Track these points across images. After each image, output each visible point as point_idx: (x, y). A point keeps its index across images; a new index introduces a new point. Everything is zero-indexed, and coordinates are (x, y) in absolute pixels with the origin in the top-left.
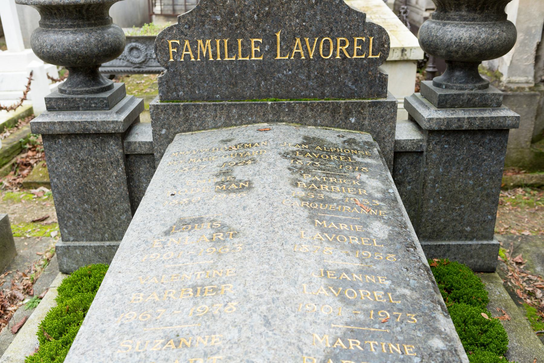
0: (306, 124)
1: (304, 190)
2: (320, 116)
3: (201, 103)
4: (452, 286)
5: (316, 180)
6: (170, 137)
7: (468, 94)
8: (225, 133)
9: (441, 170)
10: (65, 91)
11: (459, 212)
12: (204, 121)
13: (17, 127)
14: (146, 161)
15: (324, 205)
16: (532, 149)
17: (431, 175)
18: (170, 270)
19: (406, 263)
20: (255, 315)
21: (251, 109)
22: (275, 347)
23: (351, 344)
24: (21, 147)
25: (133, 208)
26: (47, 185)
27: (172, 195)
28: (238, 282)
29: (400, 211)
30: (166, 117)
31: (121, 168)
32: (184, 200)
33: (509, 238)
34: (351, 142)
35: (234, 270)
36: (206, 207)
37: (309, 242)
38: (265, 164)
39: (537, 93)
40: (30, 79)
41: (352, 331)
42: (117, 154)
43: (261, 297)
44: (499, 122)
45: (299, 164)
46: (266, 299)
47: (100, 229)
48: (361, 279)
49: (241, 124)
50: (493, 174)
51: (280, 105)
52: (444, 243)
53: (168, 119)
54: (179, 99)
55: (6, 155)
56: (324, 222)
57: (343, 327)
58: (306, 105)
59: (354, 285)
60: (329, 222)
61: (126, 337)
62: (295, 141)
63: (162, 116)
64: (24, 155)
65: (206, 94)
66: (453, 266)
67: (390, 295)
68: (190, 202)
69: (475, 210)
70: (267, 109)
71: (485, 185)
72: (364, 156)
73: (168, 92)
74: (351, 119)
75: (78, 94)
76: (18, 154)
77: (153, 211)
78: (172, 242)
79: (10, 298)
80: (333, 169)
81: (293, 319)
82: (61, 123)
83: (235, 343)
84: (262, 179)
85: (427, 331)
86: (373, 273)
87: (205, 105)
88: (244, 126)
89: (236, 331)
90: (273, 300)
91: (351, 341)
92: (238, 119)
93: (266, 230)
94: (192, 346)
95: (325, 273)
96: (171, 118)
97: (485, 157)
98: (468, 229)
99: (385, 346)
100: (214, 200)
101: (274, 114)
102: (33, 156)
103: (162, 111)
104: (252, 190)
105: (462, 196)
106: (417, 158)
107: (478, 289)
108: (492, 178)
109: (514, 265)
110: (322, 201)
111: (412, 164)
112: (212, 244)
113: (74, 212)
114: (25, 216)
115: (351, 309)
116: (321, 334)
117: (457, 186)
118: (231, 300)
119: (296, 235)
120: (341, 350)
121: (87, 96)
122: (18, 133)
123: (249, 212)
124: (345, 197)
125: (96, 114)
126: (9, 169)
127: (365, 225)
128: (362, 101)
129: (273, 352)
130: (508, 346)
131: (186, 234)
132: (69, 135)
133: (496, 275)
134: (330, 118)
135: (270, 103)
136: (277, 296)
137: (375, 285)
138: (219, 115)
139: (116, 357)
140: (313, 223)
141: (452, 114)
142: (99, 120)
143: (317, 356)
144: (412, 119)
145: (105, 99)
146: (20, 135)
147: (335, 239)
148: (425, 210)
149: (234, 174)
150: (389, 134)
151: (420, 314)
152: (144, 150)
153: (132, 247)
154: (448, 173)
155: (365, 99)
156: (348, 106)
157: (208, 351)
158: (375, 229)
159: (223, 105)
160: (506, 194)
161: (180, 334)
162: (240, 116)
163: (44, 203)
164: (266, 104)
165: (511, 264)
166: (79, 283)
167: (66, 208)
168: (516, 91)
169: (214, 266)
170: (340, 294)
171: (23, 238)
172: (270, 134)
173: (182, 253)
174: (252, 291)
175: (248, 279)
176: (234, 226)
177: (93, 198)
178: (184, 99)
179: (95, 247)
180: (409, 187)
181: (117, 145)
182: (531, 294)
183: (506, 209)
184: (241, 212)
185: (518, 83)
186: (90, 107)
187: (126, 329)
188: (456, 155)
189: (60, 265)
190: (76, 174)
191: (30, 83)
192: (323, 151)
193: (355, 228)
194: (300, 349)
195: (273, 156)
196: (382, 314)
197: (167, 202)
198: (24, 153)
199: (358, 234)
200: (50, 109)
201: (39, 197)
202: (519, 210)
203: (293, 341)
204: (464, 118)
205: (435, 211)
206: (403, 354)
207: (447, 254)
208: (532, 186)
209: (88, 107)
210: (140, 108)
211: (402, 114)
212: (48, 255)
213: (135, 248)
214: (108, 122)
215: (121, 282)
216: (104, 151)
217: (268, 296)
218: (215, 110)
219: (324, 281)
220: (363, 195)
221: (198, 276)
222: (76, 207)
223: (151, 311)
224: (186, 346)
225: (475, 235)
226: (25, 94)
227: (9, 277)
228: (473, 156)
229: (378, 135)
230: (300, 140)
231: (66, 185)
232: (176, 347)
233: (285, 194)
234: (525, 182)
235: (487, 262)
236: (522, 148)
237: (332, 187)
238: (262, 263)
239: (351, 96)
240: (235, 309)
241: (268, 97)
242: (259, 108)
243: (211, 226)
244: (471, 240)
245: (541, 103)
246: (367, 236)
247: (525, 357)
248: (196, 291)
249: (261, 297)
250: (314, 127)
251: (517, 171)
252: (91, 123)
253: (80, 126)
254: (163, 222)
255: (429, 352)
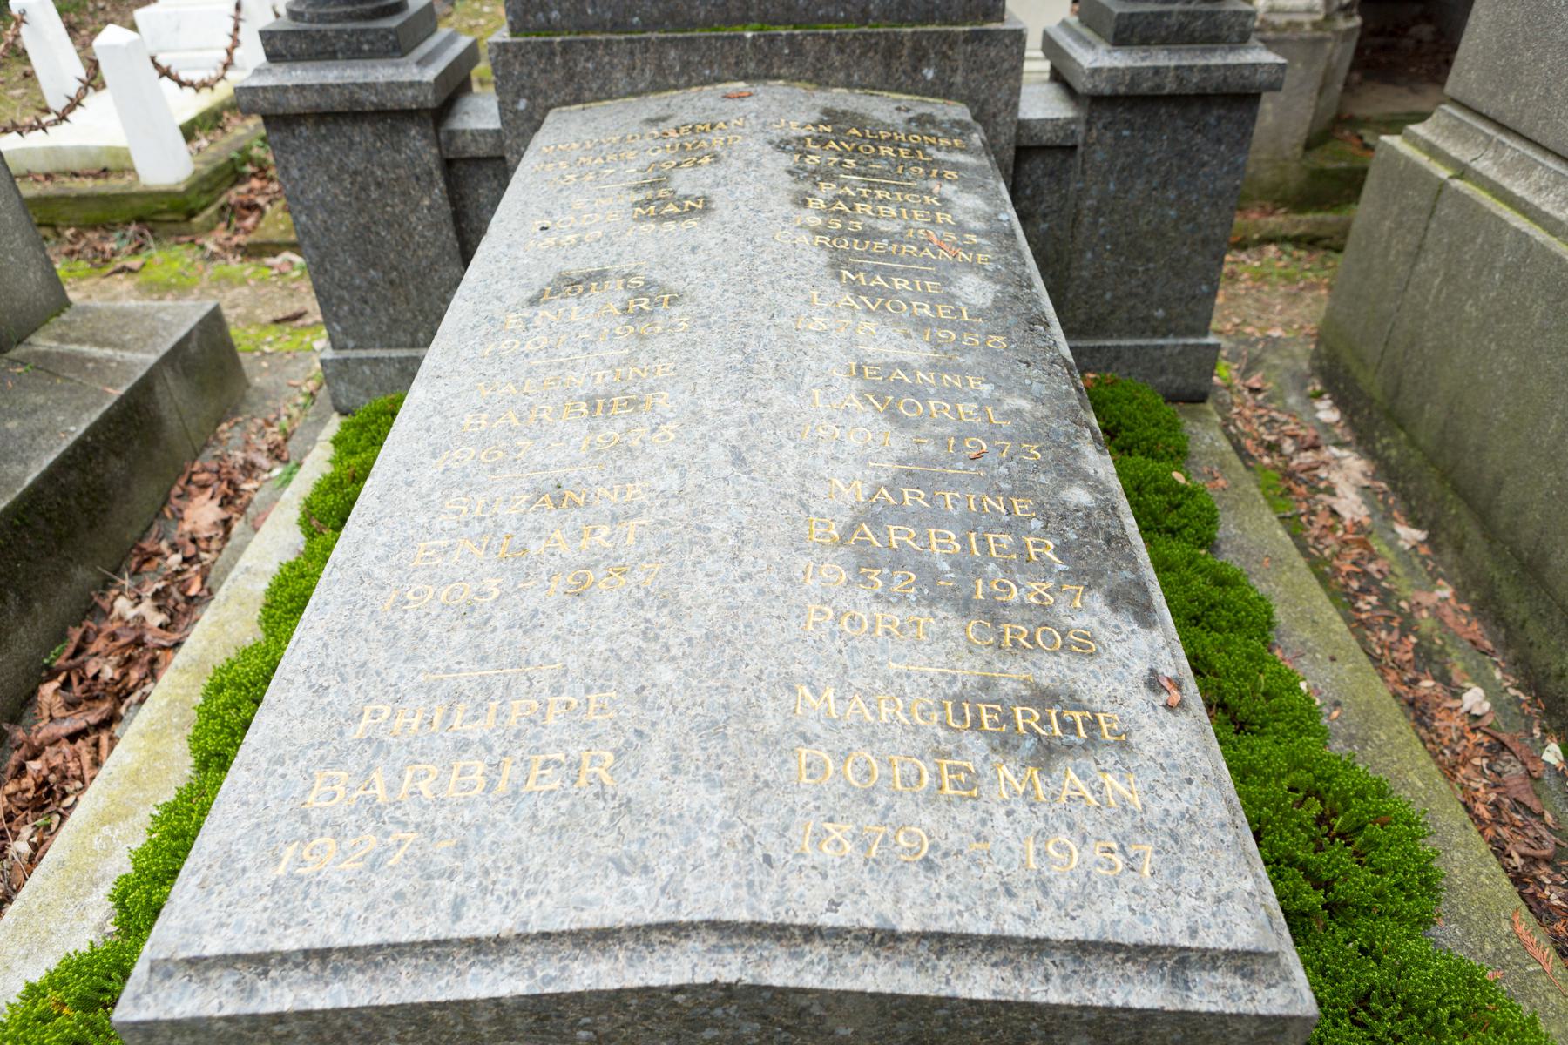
0: (827, 84)
1: (821, 213)
2: (858, 63)
3: (599, 37)
4: (1119, 424)
5: (847, 195)
6: (537, 117)
7: (1181, 13)
8: (653, 105)
9: (1112, 186)
10: (302, 14)
11: (1144, 278)
12: (608, 79)
13: (222, 128)
14: (490, 173)
15: (862, 243)
16: (1304, 163)
17: (1091, 197)
18: (542, 370)
19: (1026, 352)
20: (713, 446)
21: (709, 49)
22: (754, 501)
23: (907, 497)
24: (235, 171)
25: (466, 257)
26: (294, 247)
27: (543, 229)
28: (681, 386)
29: (1019, 254)
30: (526, 70)
31: (439, 190)
32: (569, 238)
33: (1239, 342)
34: (923, 121)
35: (672, 365)
36: (614, 249)
37: (828, 312)
38: (740, 164)
39: (1328, 34)
40: (237, 20)
41: (910, 474)
42: (427, 157)
43: (727, 412)
44: (1242, 77)
45: (812, 161)
46: (736, 416)
47: (408, 321)
48: (932, 381)
49: (688, 85)
50: (1220, 194)
51: (772, 39)
52: (1109, 343)
53: (530, 75)
54: (551, 29)
55: (206, 187)
56: (862, 275)
57: (893, 468)
58: (829, 38)
59: (918, 393)
60: (870, 274)
61: (456, 492)
62: (804, 118)
63: (517, 69)
64: (243, 189)
65: (608, 15)
66: (1124, 387)
67: (989, 410)
68: (580, 241)
69: (1177, 274)
70: (743, 49)
71: (1201, 219)
72: (950, 149)
73: (526, 12)
74: (925, 71)
75: (330, 22)
76: (232, 186)
77: (504, 260)
78: (544, 318)
79: (243, 468)
80: (882, 174)
81: (792, 452)
82: (301, 88)
83: (674, 496)
84: (732, 193)
85: (1060, 475)
86: (958, 369)
87: (608, 43)
88: (694, 89)
89: (676, 476)
90: (751, 419)
91: (906, 491)
92: (682, 73)
93: (738, 289)
94: (587, 504)
95: (860, 369)
96: (535, 74)
97: (1206, 158)
98: (1160, 313)
99: (978, 540)
100: (630, 236)
101: (760, 62)
102: (263, 188)
103: (515, 57)
104: (712, 215)
105: (1152, 244)
106: (1064, 161)
107: (1169, 429)
108: (1215, 204)
109: (1246, 393)
110: (857, 235)
111: (1051, 174)
112: (627, 319)
113: (351, 288)
114: (259, 311)
115: (908, 435)
116: (847, 478)
117: (1142, 222)
118: (665, 421)
119: (801, 298)
120: (886, 506)
121: (350, 26)
122: (225, 140)
123: (703, 257)
124: (907, 227)
125: (373, 67)
126: (215, 218)
127: (945, 281)
128: (950, 28)
129: (749, 510)
130: (1219, 534)
131: (572, 302)
132: (322, 117)
133: (1209, 406)
134: (880, 69)
135: (749, 35)
136: (761, 410)
137: (961, 392)
138: (639, 64)
139: (438, 526)
140: (839, 276)
141: (1143, 59)
142: (381, 80)
143: (837, 517)
144: (1057, 76)
145: (390, 31)
146: (229, 145)
147: (882, 307)
148: (1074, 274)
149: (673, 185)
150: (1007, 104)
151: (1049, 443)
152: (483, 149)
153: (462, 331)
154: (1127, 192)
155: (955, 24)
156: (919, 41)
157: (619, 511)
158: (967, 289)
159: (647, 40)
160: (1243, 256)
161: (564, 483)
162: (686, 65)
163: (293, 286)
164: (742, 38)
165: (1240, 392)
166: (373, 427)
167: (332, 278)
168: (1284, 30)
169: (631, 359)
170: (890, 407)
171: (257, 354)
172: (750, 104)
173: (564, 337)
174: (708, 402)
175: (700, 381)
176: (673, 284)
177: (387, 256)
178: (563, 28)
179: (400, 360)
180: (1044, 226)
181: (425, 136)
182: (1272, 448)
183: (1241, 288)
184: (687, 258)
185: (1290, 12)
186: (360, 50)
187: (456, 477)
188: (1144, 154)
189: (334, 398)
190: (345, 204)
191: (237, 29)
192: (864, 137)
193: (924, 287)
194: (803, 506)
195: (755, 146)
196: (972, 443)
197: (532, 243)
198: (243, 183)
199: (933, 300)
200: (273, 56)
201: (282, 274)
202: (1266, 288)
203: (789, 491)
204: (1168, 68)
205: (1094, 276)
206: (1009, 514)
207: (1115, 366)
208: (1297, 241)
209: (355, 53)
210: (470, 56)
211: (1036, 65)
212: (311, 385)
213: (468, 331)
214: (401, 85)
215: (443, 395)
216: (399, 152)
217: (741, 411)
218: (632, 53)
219: (857, 384)
220: (945, 225)
221: (599, 380)
222: (352, 278)
223: (503, 444)
224: (576, 505)
225: (1173, 325)
226: (230, 53)
227: (237, 429)
228: (1181, 155)
229: (982, 110)
230: (815, 115)
231: (327, 229)
232: (556, 506)
233: (780, 220)
234: (1283, 232)
235: (1191, 381)
236: (1285, 159)
237: (881, 208)
238: (727, 351)
239: (927, 19)
240: (673, 436)
241: (745, 21)
242: (727, 47)
243: (625, 286)
244: (1165, 336)
245: (1335, 59)
246: (949, 303)
247: (1248, 554)
248: (595, 406)
249: (727, 412)
250: (845, 91)
251: (1269, 208)
252: (365, 86)
253: (341, 94)
254: (524, 281)
255: (1062, 510)
